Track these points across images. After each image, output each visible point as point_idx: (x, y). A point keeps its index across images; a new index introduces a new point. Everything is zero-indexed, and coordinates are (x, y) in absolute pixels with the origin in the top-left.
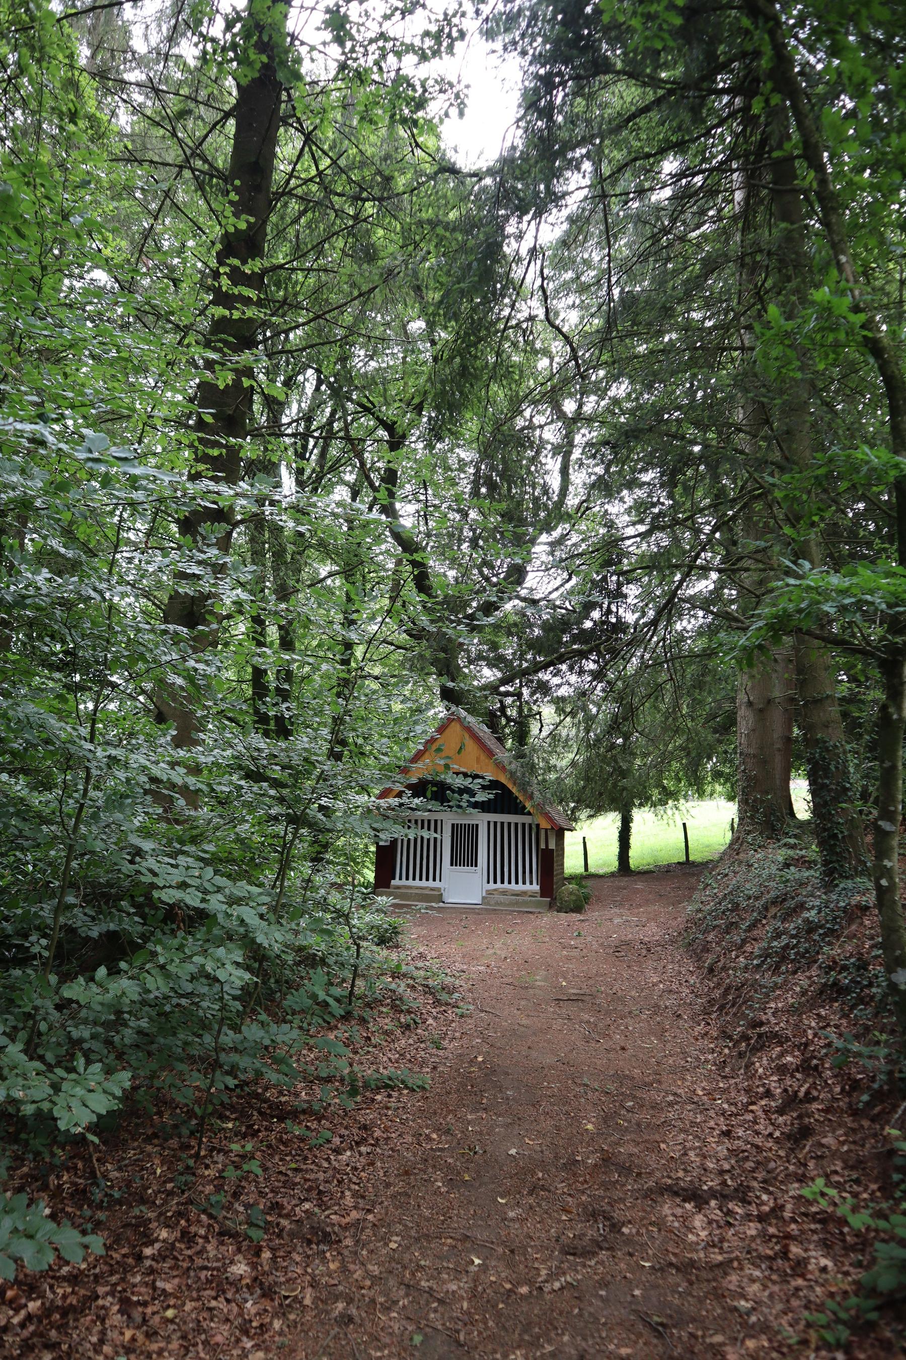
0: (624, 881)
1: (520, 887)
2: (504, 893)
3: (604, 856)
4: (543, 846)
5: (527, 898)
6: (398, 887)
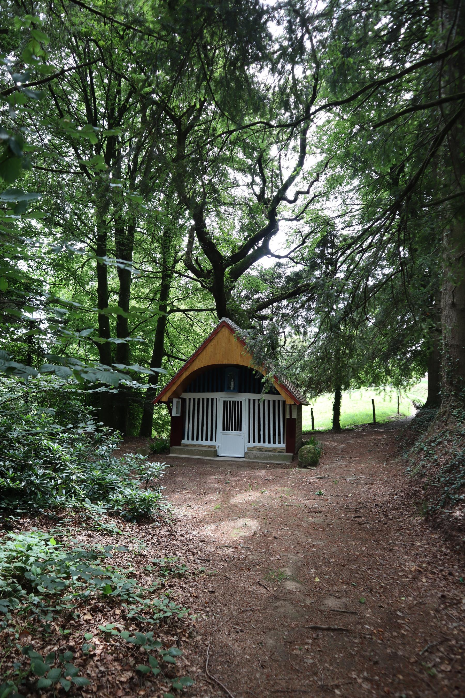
0: (340, 437)
1: (272, 445)
2: (260, 449)
3: (324, 421)
4: (288, 416)
5: (276, 454)
6: (186, 445)
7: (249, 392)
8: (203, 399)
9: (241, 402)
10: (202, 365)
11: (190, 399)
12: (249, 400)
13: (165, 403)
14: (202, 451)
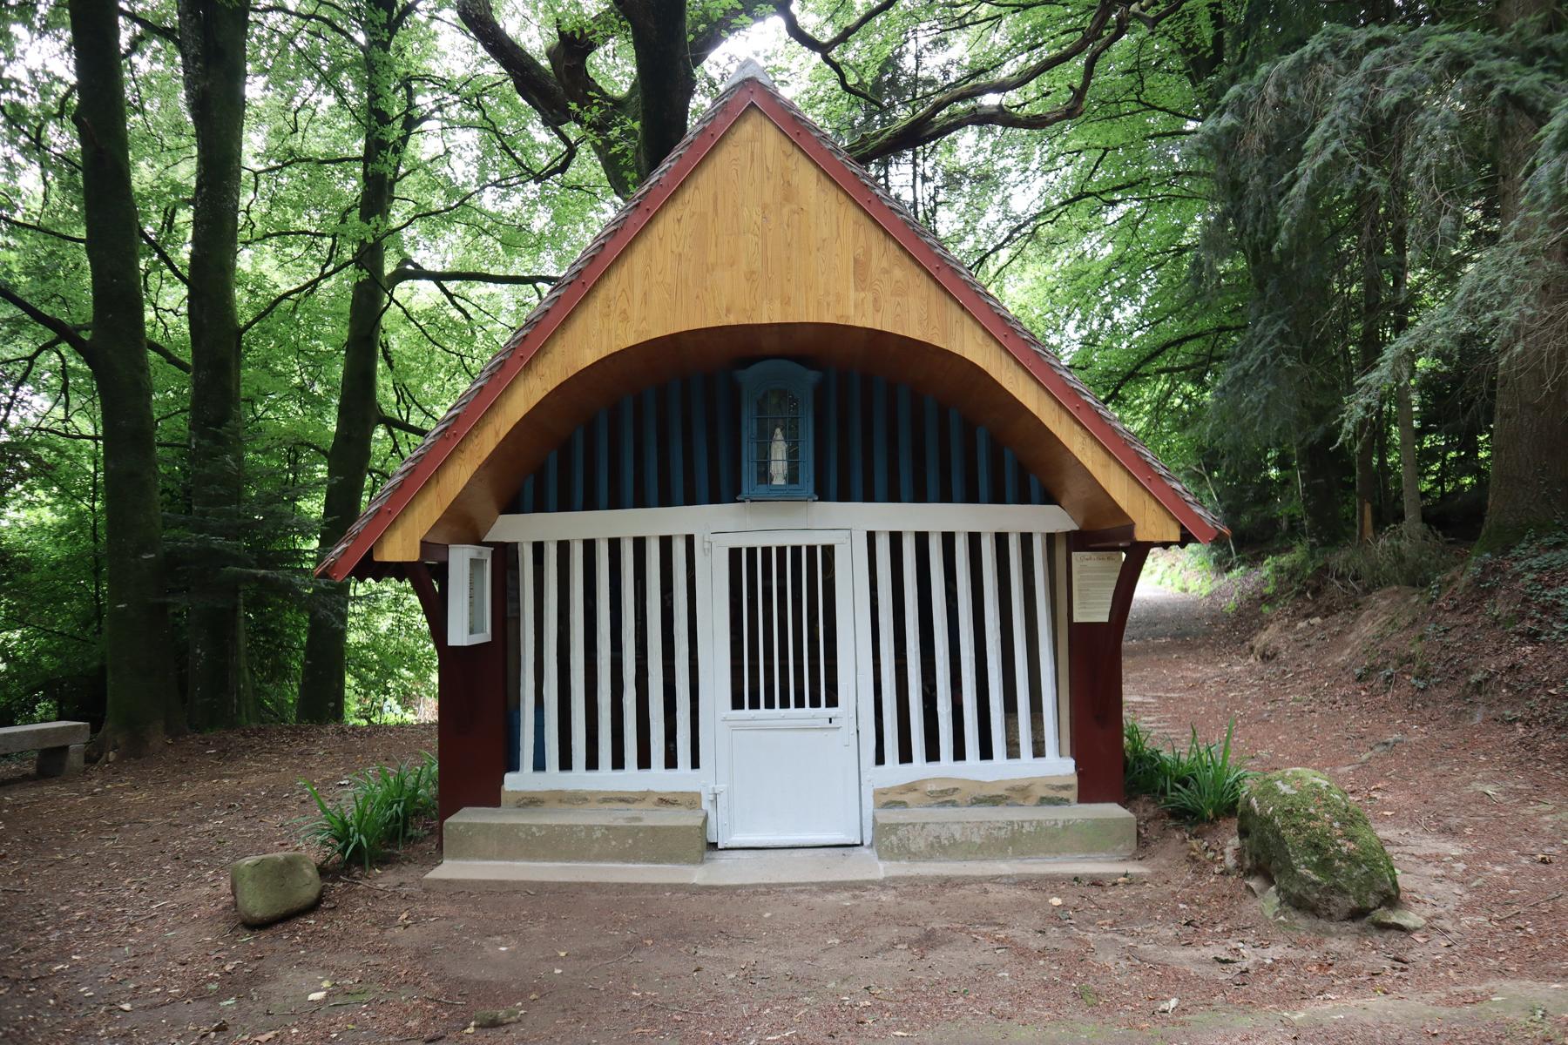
2: (945, 797)
6: (531, 802)
7: (869, 497)
8: (615, 545)
9: (829, 551)
10: (628, 338)
11: (538, 548)
12: (871, 536)
13: (398, 570)
14: (633, 832)
